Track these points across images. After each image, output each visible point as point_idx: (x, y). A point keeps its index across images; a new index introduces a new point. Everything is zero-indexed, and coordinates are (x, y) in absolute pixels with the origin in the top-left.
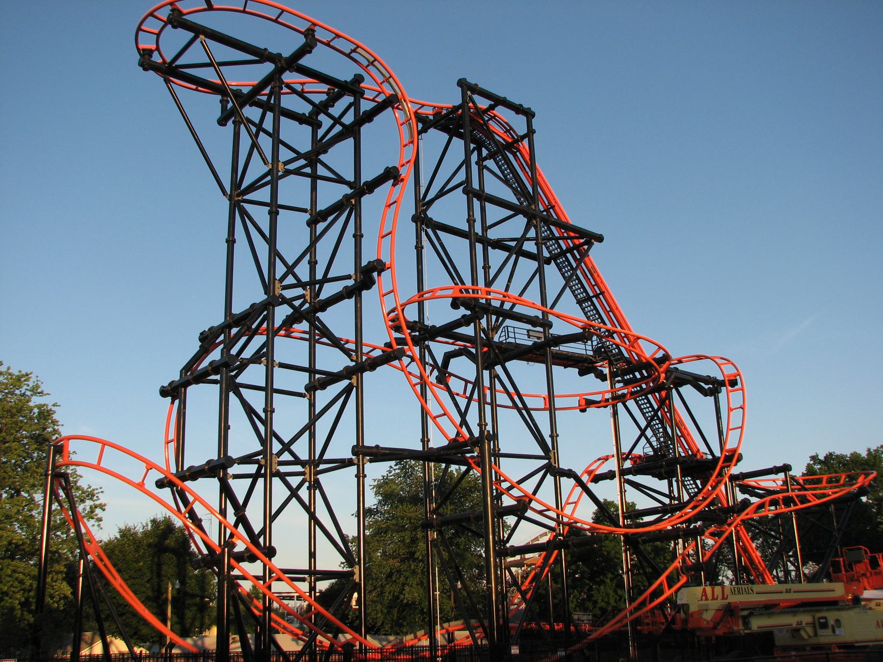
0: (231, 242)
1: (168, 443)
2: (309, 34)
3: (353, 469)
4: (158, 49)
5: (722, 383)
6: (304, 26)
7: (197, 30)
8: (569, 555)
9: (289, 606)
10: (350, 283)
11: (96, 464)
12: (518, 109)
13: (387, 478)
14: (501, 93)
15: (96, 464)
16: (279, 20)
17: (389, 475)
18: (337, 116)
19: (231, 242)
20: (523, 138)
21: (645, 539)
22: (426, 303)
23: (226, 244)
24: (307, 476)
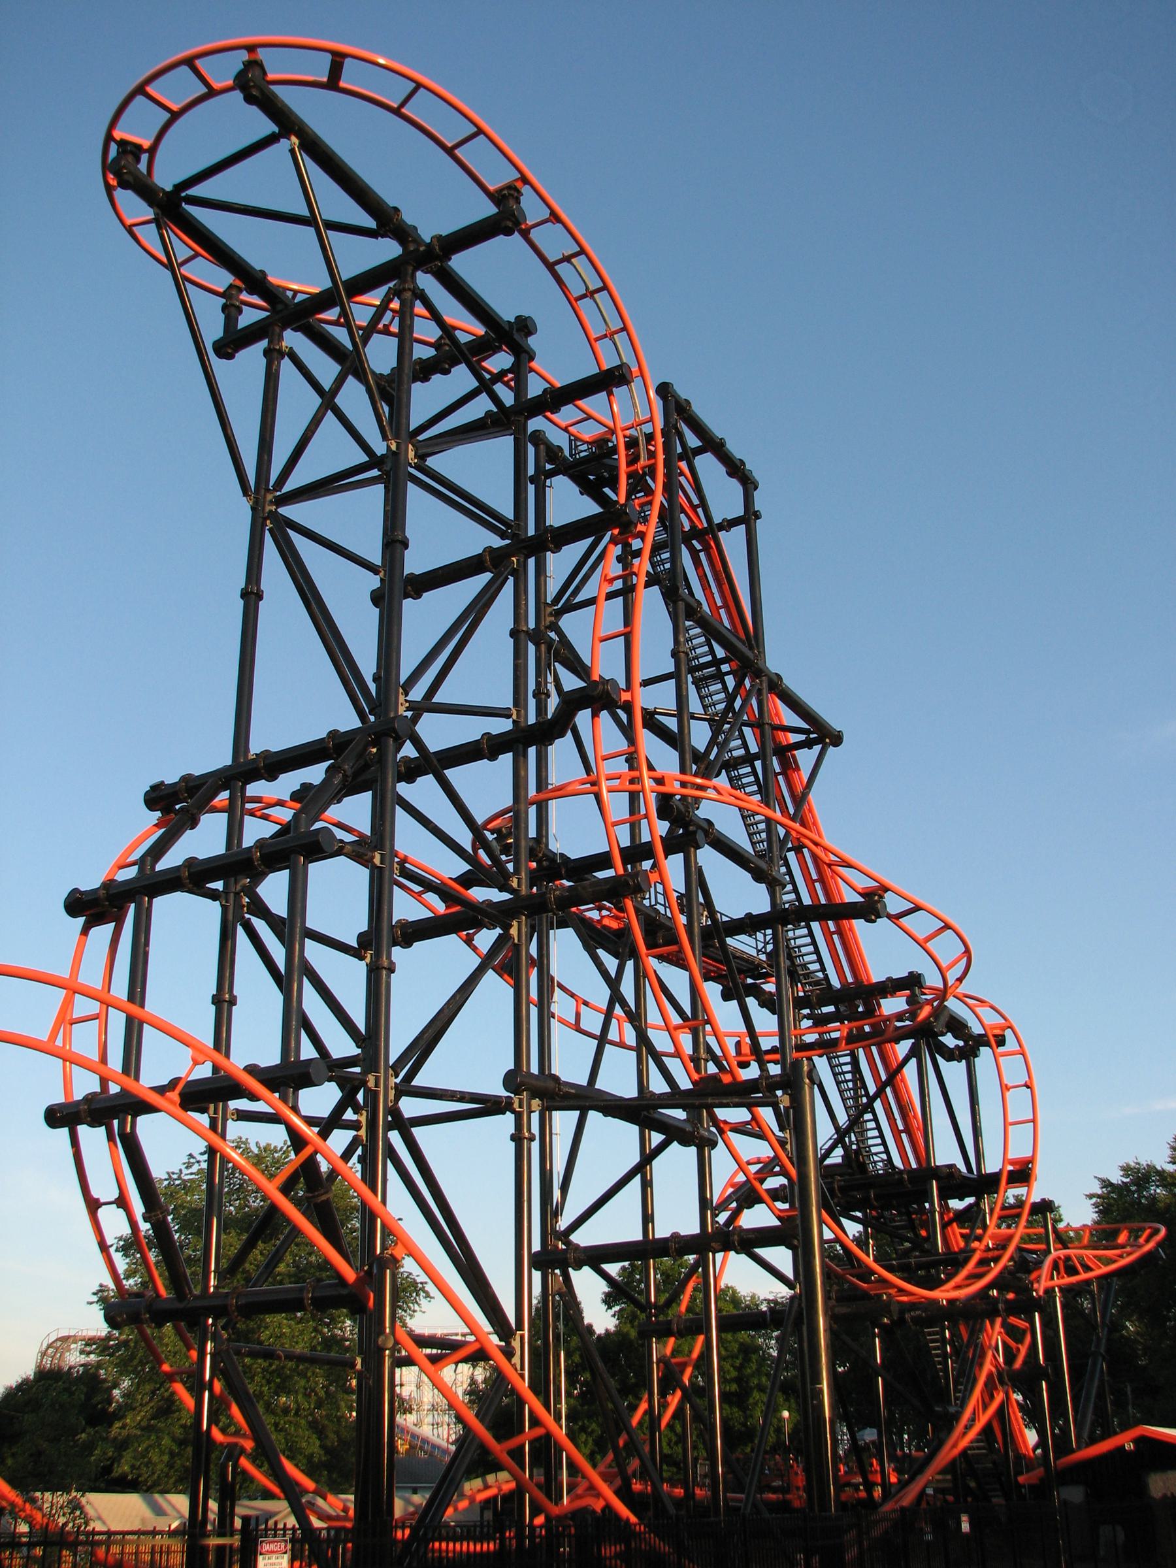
0: (252, 596)
1: (72, 1024)
2: (506, 197)
3: (506, 1122)
4: (152, 150)
5: (982, 1041)
6: (498, 177)
8: (578, 1353)
9: (407, 1420)
10: (501, 726)
11: (45, 1038)
12: (736, 469)
13: (179, 1178)
14: (718, 429)
15: (45, 1038)
16: (457, 152)
17: (185, 1171)
18: (484, 397)
19: (252, 596)
21: (919, 1316)
22: (552, 804)
23: (242, 602)
24: (363, 1132)
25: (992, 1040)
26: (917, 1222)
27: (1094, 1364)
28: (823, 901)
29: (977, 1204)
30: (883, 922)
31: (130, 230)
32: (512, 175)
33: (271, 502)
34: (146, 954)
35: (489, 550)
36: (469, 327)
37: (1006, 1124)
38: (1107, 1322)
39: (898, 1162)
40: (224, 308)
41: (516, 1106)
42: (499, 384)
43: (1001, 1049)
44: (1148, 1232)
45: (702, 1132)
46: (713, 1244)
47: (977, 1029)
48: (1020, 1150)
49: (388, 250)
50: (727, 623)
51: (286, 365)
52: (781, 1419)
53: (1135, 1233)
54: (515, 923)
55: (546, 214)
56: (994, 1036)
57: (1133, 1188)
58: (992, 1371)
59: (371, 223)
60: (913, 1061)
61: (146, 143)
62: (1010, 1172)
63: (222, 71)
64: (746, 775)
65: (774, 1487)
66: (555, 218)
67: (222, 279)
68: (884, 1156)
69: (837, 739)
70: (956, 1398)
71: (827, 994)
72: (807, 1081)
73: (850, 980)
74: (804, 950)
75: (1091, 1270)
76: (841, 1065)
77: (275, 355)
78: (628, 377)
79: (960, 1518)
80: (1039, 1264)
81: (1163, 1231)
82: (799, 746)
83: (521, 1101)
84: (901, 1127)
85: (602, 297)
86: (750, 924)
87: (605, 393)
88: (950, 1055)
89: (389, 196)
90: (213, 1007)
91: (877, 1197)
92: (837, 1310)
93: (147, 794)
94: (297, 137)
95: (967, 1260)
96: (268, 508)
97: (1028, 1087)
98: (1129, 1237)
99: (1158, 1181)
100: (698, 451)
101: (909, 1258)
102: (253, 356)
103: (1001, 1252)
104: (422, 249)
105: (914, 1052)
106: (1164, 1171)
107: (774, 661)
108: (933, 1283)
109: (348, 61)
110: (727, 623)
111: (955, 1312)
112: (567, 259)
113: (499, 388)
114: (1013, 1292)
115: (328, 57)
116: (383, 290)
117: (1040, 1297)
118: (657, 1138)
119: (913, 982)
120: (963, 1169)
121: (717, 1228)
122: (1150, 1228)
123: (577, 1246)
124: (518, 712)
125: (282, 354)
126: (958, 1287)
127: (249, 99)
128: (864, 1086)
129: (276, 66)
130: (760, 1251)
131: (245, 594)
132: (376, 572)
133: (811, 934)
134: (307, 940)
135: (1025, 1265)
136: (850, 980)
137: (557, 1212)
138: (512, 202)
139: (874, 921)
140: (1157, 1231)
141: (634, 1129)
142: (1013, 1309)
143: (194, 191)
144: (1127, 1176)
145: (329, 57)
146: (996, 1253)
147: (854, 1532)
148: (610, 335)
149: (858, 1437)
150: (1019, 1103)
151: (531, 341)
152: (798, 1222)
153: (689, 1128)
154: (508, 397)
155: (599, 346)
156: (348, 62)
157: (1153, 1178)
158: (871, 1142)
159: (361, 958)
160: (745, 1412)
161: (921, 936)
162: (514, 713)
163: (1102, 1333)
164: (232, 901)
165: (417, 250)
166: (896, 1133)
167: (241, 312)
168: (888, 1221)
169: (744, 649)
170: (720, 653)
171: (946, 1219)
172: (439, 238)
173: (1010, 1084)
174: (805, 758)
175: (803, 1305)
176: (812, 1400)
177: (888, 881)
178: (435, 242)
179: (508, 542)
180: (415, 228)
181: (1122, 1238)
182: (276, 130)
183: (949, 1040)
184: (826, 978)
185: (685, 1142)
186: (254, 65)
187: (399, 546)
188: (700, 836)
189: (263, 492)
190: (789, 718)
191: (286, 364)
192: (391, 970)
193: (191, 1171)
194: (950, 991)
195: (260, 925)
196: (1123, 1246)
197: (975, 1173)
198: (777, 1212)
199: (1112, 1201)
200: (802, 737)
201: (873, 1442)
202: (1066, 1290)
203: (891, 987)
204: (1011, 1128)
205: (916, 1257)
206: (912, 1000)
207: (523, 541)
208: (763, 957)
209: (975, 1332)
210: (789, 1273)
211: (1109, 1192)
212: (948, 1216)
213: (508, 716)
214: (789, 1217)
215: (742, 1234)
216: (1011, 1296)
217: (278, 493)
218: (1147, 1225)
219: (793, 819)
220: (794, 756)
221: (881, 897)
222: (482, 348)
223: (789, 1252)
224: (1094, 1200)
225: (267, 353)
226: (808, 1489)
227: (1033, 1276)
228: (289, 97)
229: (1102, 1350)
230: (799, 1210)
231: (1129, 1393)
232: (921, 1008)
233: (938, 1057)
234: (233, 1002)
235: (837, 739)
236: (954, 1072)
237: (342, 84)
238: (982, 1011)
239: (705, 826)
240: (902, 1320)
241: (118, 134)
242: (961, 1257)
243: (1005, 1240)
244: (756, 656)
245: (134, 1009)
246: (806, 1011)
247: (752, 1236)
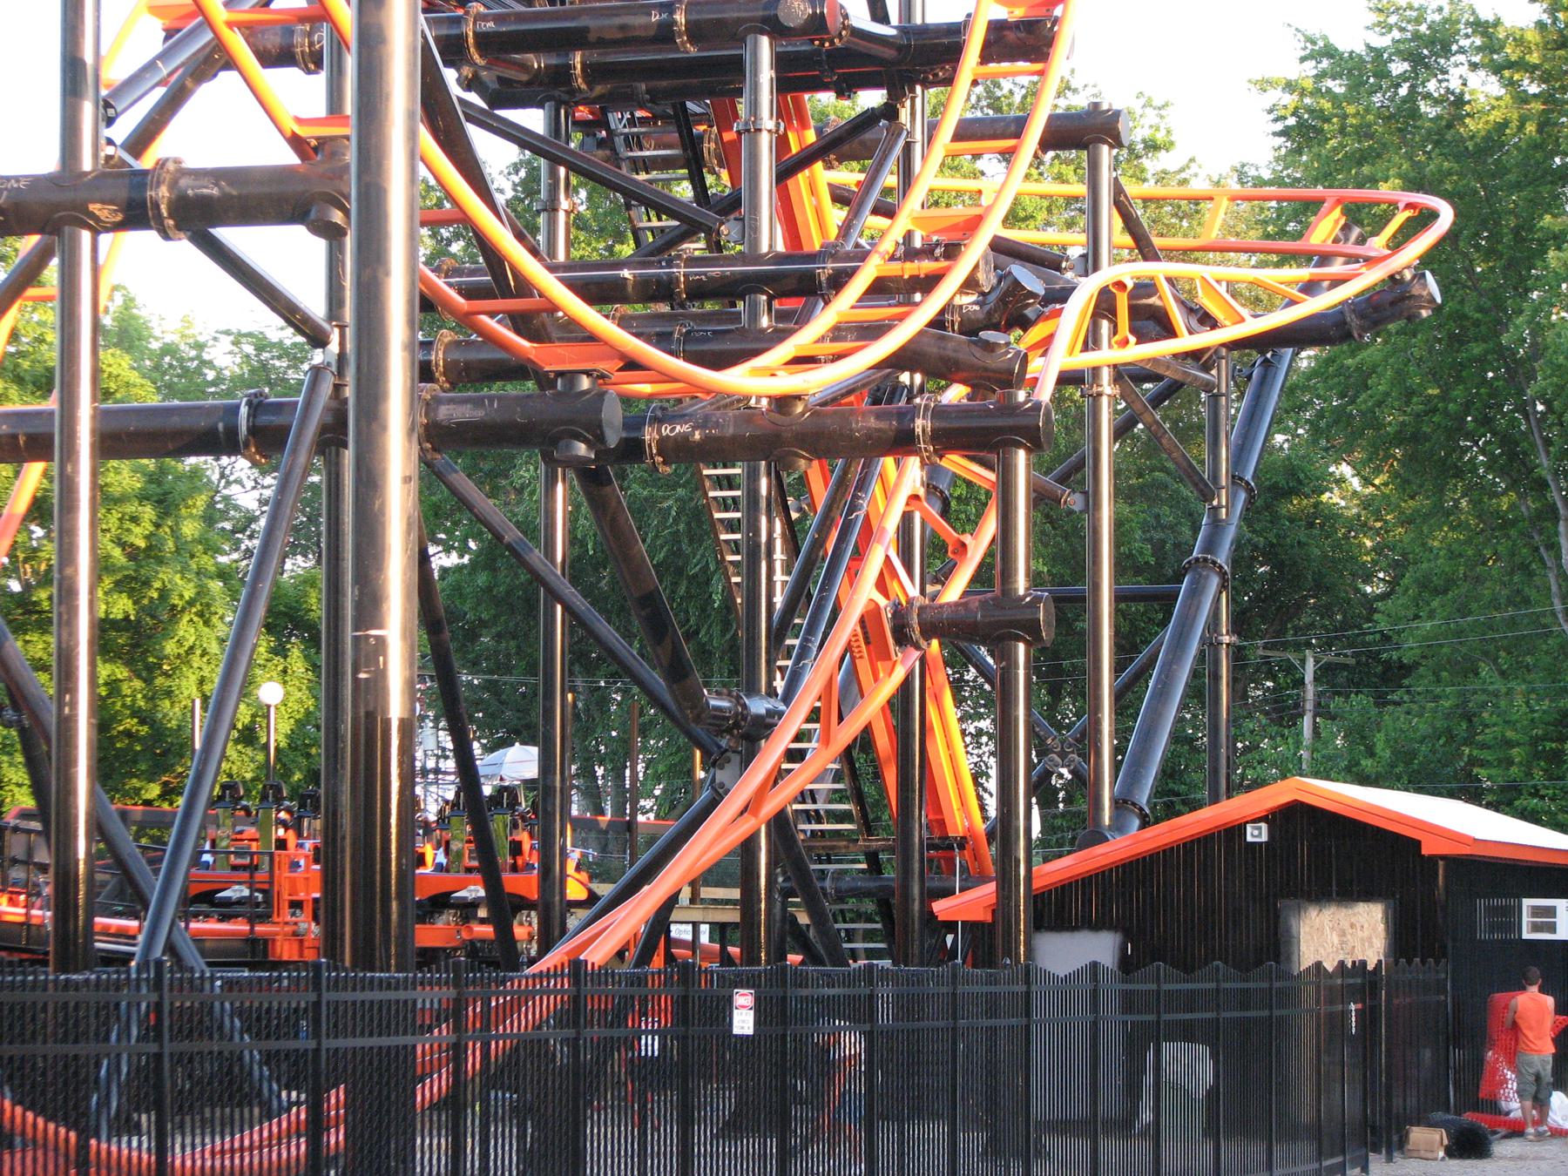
21: (685, 438)
26: (709, 147)
27: (1196, 592)
29: (889, 112)
38: (1248, 477)
46: (94, 208)
58: (877, 606)
65: (228, 903)
79: (730, 1000)
81: (1446, 215)
91: (594, 72)
92: (444, 413)
95: (839, 281)
99: (1479, 49)
101: (670, 264)
103: (943, 264)
114: (964, 382)
117: (1037, 407)
121: (109, 158)
122: (1409, 206)
126: (803, 361)
130: (228, 235)
140: (1430, 216)
146: (926, 266)
147: (444, 1032)
149: (482, 771)
152: (351, 157)
157: (1463, 42)
160: (148, 681)
163: (1229, 506)
168: (619, 141)
171: (795, 149)
175: (349, 392)
176: (356, 671)
196: (1325, 258)
197: (894, 20)
198: (290, 126)
199: (1326, 105)
201: (529, 784)
202: (1128, 375)
205: (692, 261)
209: (848, 492)
210: (314, 303)
212: (801, 139)
214: (323, 142)
215: (183, 182)
216: (956, 394)
223: (319, 245)
226: (327, 911)
229: (1223, 558)
230: (353, 121)
231: (1309, 677)
240: (632, 449)
242: (826, 269)
243: (953, 228)
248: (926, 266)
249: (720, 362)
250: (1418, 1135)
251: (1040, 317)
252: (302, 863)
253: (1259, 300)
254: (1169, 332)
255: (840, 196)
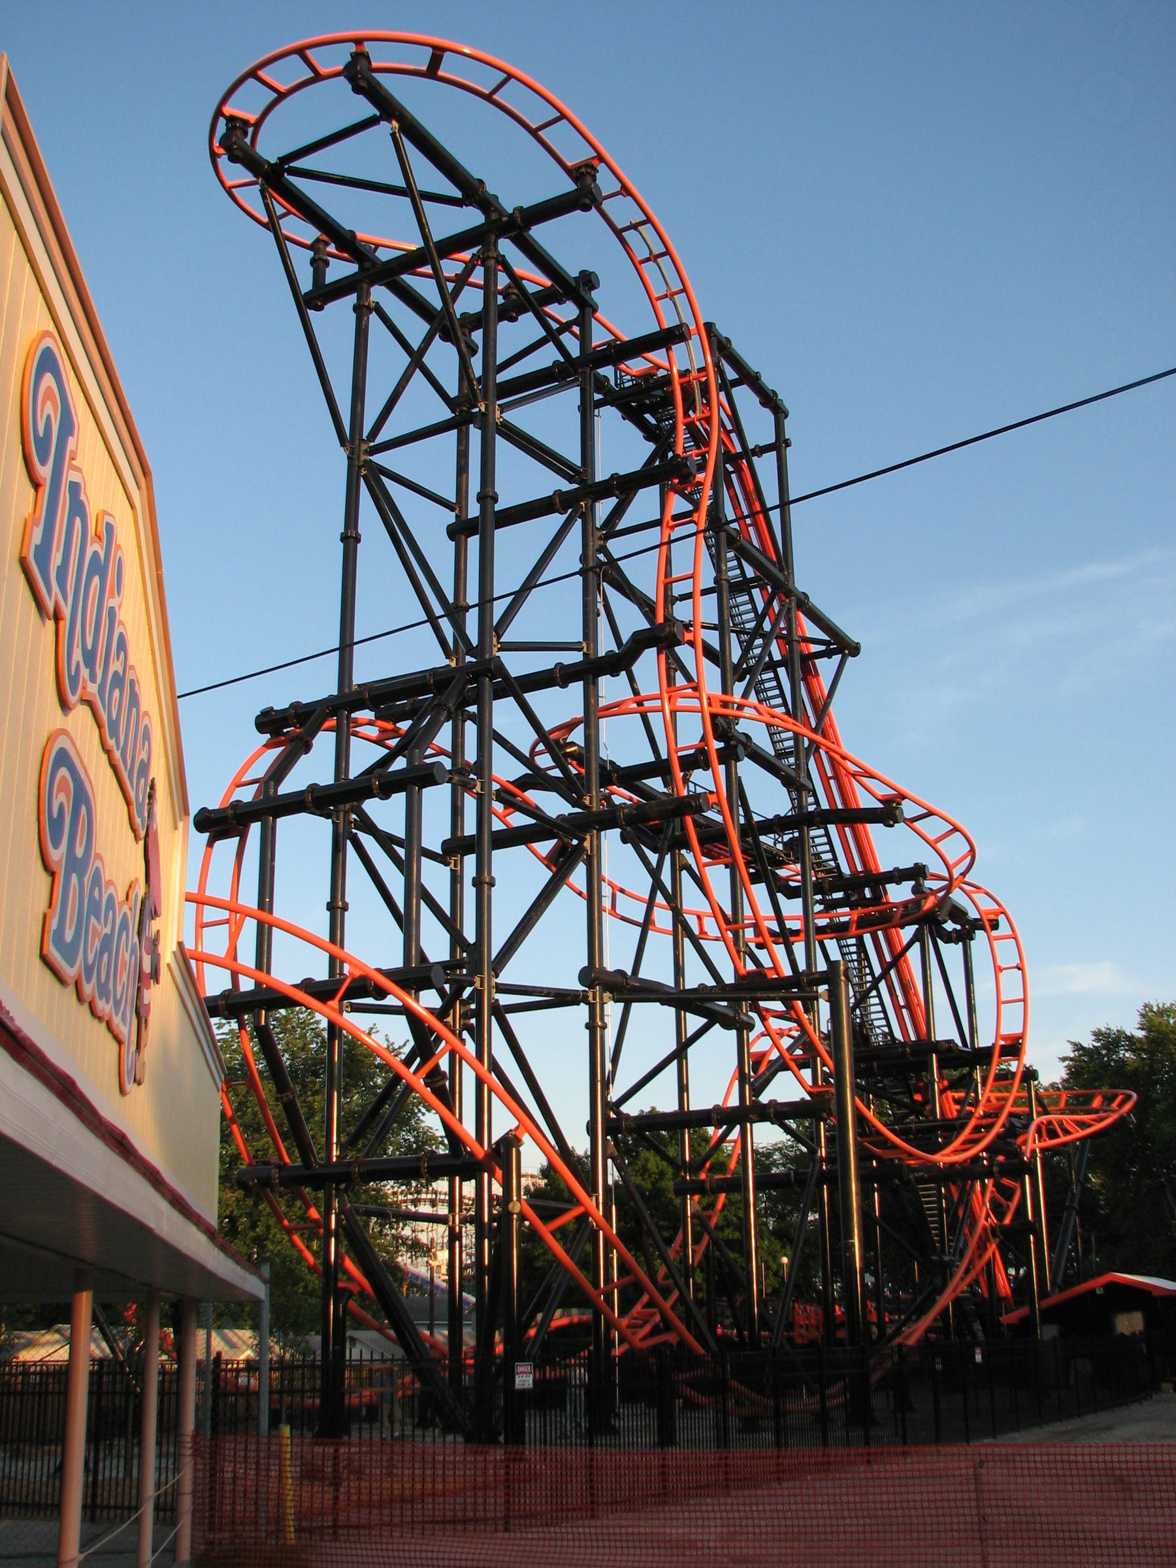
0: (350, 539)
2: (582, 174)
4: (258, 125)
5: (977, 925)
6: (577, 154)
7: (387, 108)
10: (575, 657)
12: (769, 400)
14: (753, 363)
16: (541, 133)
18: (550, 346)
19: (350, 539)
20: (762, 450)
25: (987, 924)
27: (1068, 1218)
28: (840, 806)
30: (900, 827)
31: (229, 191)
32: (589, 154)
33: (366, 452)
34: (273, 868)
35: (558, 493)
36: (535, 279)
37: (999, 1003)
39: (898, 1035)
40: (313, 262)
41: (591, 999)
42: (567, 333)
43: (994, 933)
44: (1120, 1097)
45: (742, 1017)
47: (973, 914)
48: (1011, 1027)
49: (472, 217)
50: (755, 543)
51: (374, 319)
52: (781, 1265)
53: (1109, 1099)
54: (588, 837)
55: (617, 187)
56: (989, 921)
57: (1104, 1052)
59: (457, 194)
60: (917, 945)
61: (253, 117)
62: (1002, 1046)
63: (334, 59)
64: (769, 680)
66: (625, 191)
67: (308, 233)
68: (886, 1029)
69: (855, 650)
70: (950, 1247)
71: (839, 881)
72: (843, 978)
73: (860, 868)
74: (817, 841)
75: (1070, 1133)
76: (848, 946)
77: (365, 310)
78: (687, 335)
80: (1026, 1127)
82: (819, 655)
83: (594, 994)
84: (902, 1003)
85: (665, 261)
86: (776, 825)
87: (664, 350)
88: (949, 938)
89: (474, 168)
90: (328, 913)
93: (258, 717)
94: (397, 121)
95: (963, 1127)
96: (363, 457)
97: (1019, 969)
98: (1103, 1103)
100: (735, 383)
102: (342, 309)
104: (505, 219)
105: (918, 937)
106: (1133, 1036)
107: (801, 583)
108: (936, 1149)
109: (447, 55)
110: (755, 543)
111: (952, 1174)
112: (634, 227)
113: (565, 337)
115: (429, 51)
116: (467, 255)
118: (694, 1022)
119: (917, 873)
120: (959, 1044)
123: (627, 1116)
124: (588, 645)
125: (370, 310)
126: (955, 1152)
127: (357, 89)
128: (870, 966)
129: (379, 56)
131: (344, 538)
132: (452, 510)
133: (827, 835)
134: (423, 858)
135: (1013, 1131)
136: (860, 868)
137: (607, 1083)
138: (589, 180)
139: (892, 826)
140: (1129, 1097)
141: (672, 1011)
142: (1007, 1171)
143: (298, 164)
144: (1098, 1040)
145: (430, 50)
148: (670, 296)
150: (1011, 984)
151: (594, 293)
153: (731, 1013)
154: (573, 346)
155: (659, 304)
156: (447, 55)
158: (873, 1016)
159: (447, 864)
161: (932, 837)
162: (584, 645)
164: (342, 818)
165: (500, 220)
166: (897, 1008)
167: (327, 264)
169: (776, 571)
170: (750, 572)
172: (520, 209)
173: (1003, 966)
174: (826, 667)
177: (905, 788)
178: (517, 213)
179: (575, 486)
180: (496, 197)
181: (1096, 1103)
182: (378, 113)
183: (949, 926)
184: (838, 866)
185: (727, 1026)
186: (360, 57)
187: (490, 501)
188: (740, 750)
189: (357, 442)
190: (811, 630)
191: (374, 318)
192: (492, 884)
193: (222, 1031)
194: (955, 883)
195: (367, 840)
196: (1096, 1111)
200: (823, 648)
202: (1042, 1150)
203: (898, 876)
204: (1003, 1006)
206: (917, 890)
207: (590, 486)
208: (780, 847)
211: (1080, 1055)
213: (579, 650)
217: (372, 444)
218: (1119, 1091)
219: (815, 731)
220: (814, 665)
221: (899, 804)
222: (548, 297)
224: (1067, 1063)
225: (356, 308)
227: (1020, 1140)
228: (387, 82)
229: (1076, 1205)
232: (926, 898)
233: (939, 940)
234: (345, 908)
235: (855, 650)
236: (952, 952)
237: (441, 73)
238: (978, 897)
239: (743, 739)
241: (228, 110)
244: (787, 578)
245: (264, 915)
246: (819, 897)
247: (786, 1109)
248: (990, 1120)
249: (933, 1153)
250: (1164, 1386)
251: (1021, 1134)
252: (394, 1231)
253: (1083, 1125)
254: (1058, 1136)
255: (956, 1101)
